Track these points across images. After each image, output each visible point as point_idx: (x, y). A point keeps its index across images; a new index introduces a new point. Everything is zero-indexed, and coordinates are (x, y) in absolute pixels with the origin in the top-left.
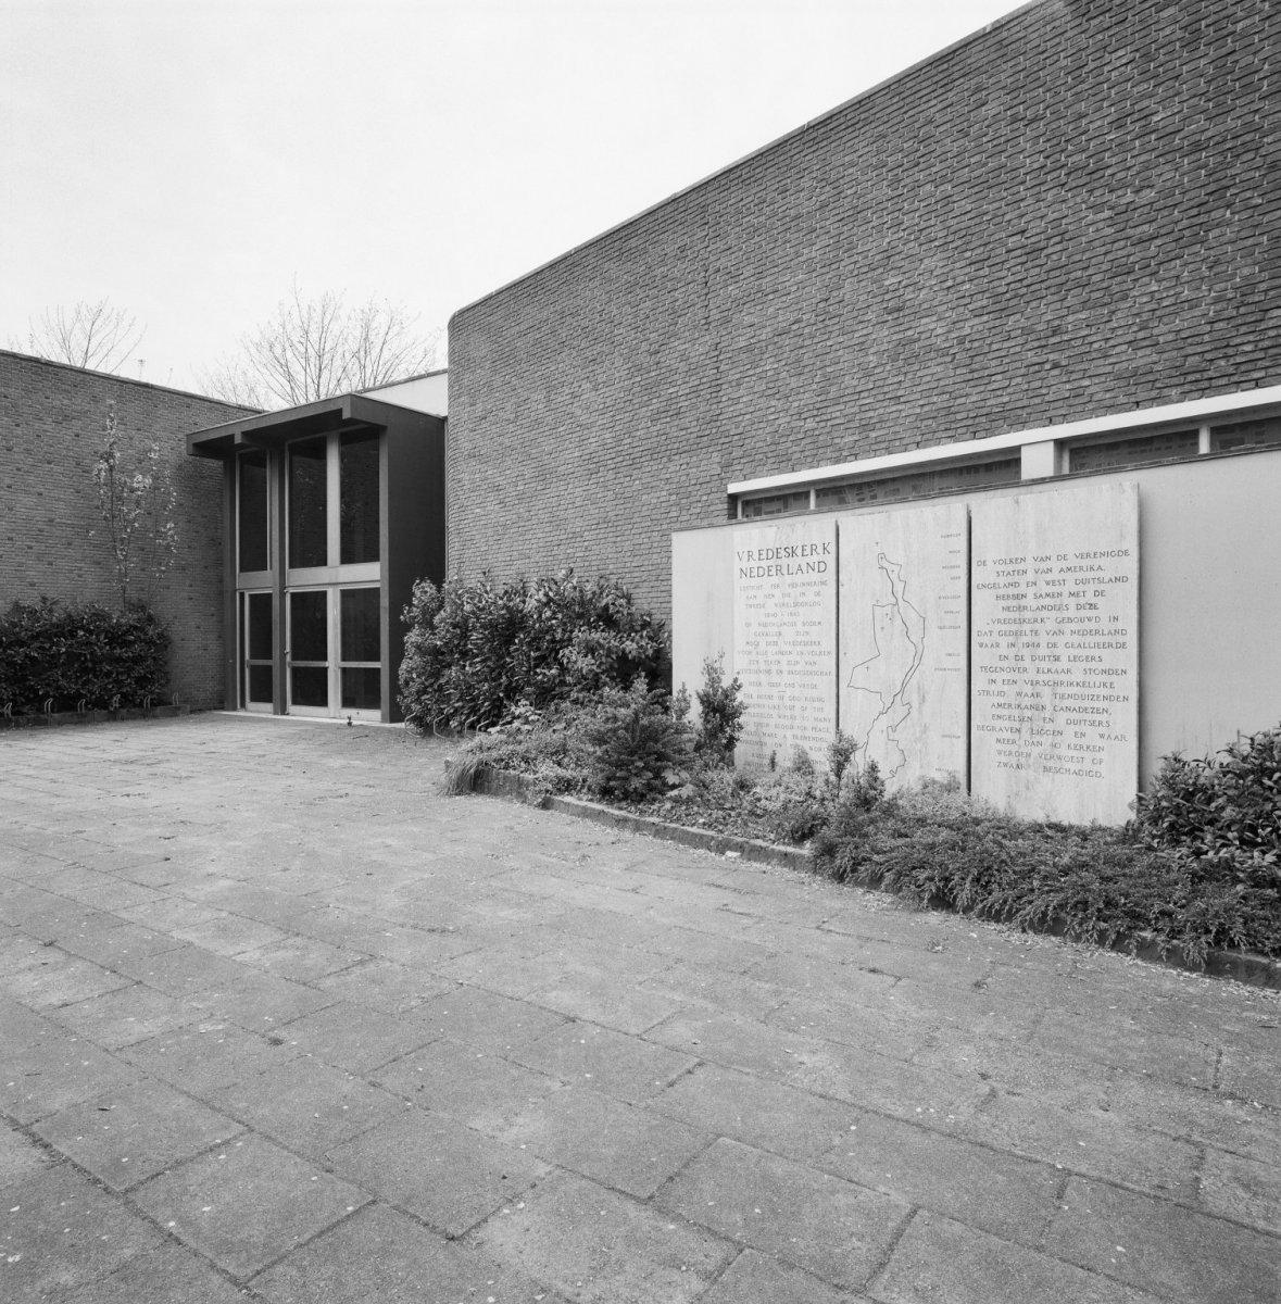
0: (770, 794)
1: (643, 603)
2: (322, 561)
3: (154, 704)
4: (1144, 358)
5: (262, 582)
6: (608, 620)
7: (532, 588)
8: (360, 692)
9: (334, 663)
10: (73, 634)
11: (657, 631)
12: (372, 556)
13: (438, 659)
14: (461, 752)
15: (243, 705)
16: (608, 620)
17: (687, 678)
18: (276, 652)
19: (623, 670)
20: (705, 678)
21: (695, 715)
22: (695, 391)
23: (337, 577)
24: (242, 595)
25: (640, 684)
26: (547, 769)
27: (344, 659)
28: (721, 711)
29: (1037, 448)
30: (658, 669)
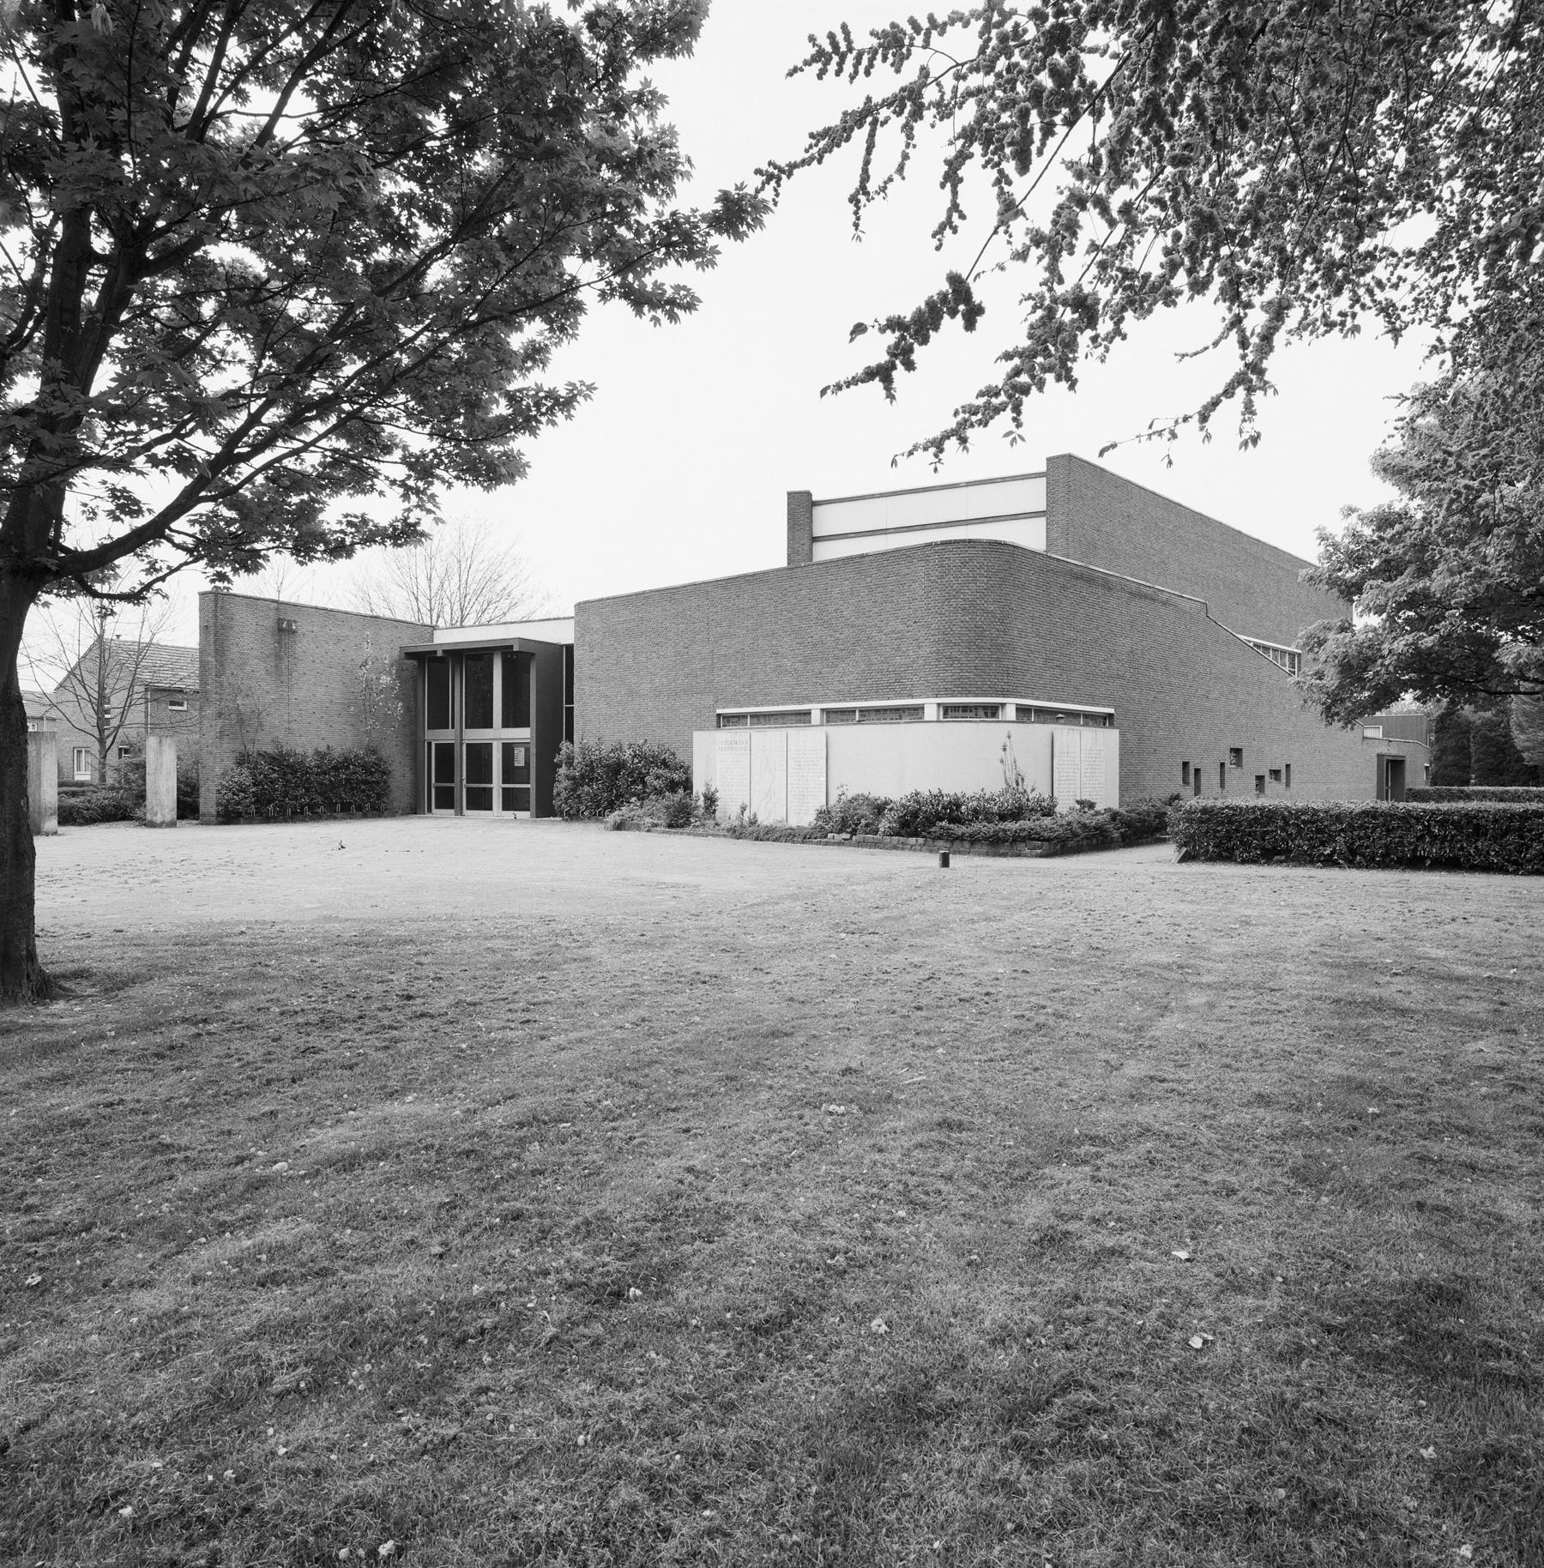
0: (725, 825)
1: (680, 757)
2: (488, 724)
3: (294, 813)
4: (841, 687)
5: (446, 736)
6: (665, 764)
7: (625, 747)
8: (513, 802)
9: (497, 785)
10: (347, 768)
11: (687, 770)
12: (526, 724)
13: (577, 782)
14: (614, 817)
15: (430, 811)
16: (665, 764)
17: (699, 788)
18: (457, 779)
19: (673, 786)
20: (1075, 374)
21: (701, 802)
22: (703, 668)
23: (497, 735)
24: (430, 744)
25: (681, 791)
26: (648, 820)
27: (504, 782)
28: (711, 800)
29: (815, 709)
30: (687, 785)
